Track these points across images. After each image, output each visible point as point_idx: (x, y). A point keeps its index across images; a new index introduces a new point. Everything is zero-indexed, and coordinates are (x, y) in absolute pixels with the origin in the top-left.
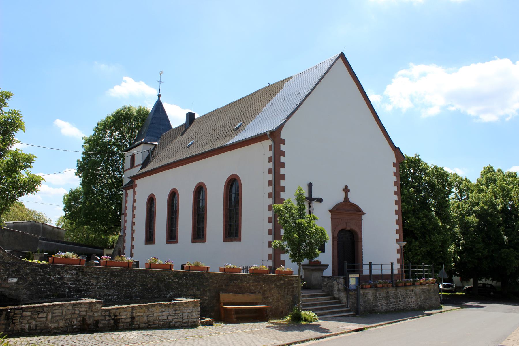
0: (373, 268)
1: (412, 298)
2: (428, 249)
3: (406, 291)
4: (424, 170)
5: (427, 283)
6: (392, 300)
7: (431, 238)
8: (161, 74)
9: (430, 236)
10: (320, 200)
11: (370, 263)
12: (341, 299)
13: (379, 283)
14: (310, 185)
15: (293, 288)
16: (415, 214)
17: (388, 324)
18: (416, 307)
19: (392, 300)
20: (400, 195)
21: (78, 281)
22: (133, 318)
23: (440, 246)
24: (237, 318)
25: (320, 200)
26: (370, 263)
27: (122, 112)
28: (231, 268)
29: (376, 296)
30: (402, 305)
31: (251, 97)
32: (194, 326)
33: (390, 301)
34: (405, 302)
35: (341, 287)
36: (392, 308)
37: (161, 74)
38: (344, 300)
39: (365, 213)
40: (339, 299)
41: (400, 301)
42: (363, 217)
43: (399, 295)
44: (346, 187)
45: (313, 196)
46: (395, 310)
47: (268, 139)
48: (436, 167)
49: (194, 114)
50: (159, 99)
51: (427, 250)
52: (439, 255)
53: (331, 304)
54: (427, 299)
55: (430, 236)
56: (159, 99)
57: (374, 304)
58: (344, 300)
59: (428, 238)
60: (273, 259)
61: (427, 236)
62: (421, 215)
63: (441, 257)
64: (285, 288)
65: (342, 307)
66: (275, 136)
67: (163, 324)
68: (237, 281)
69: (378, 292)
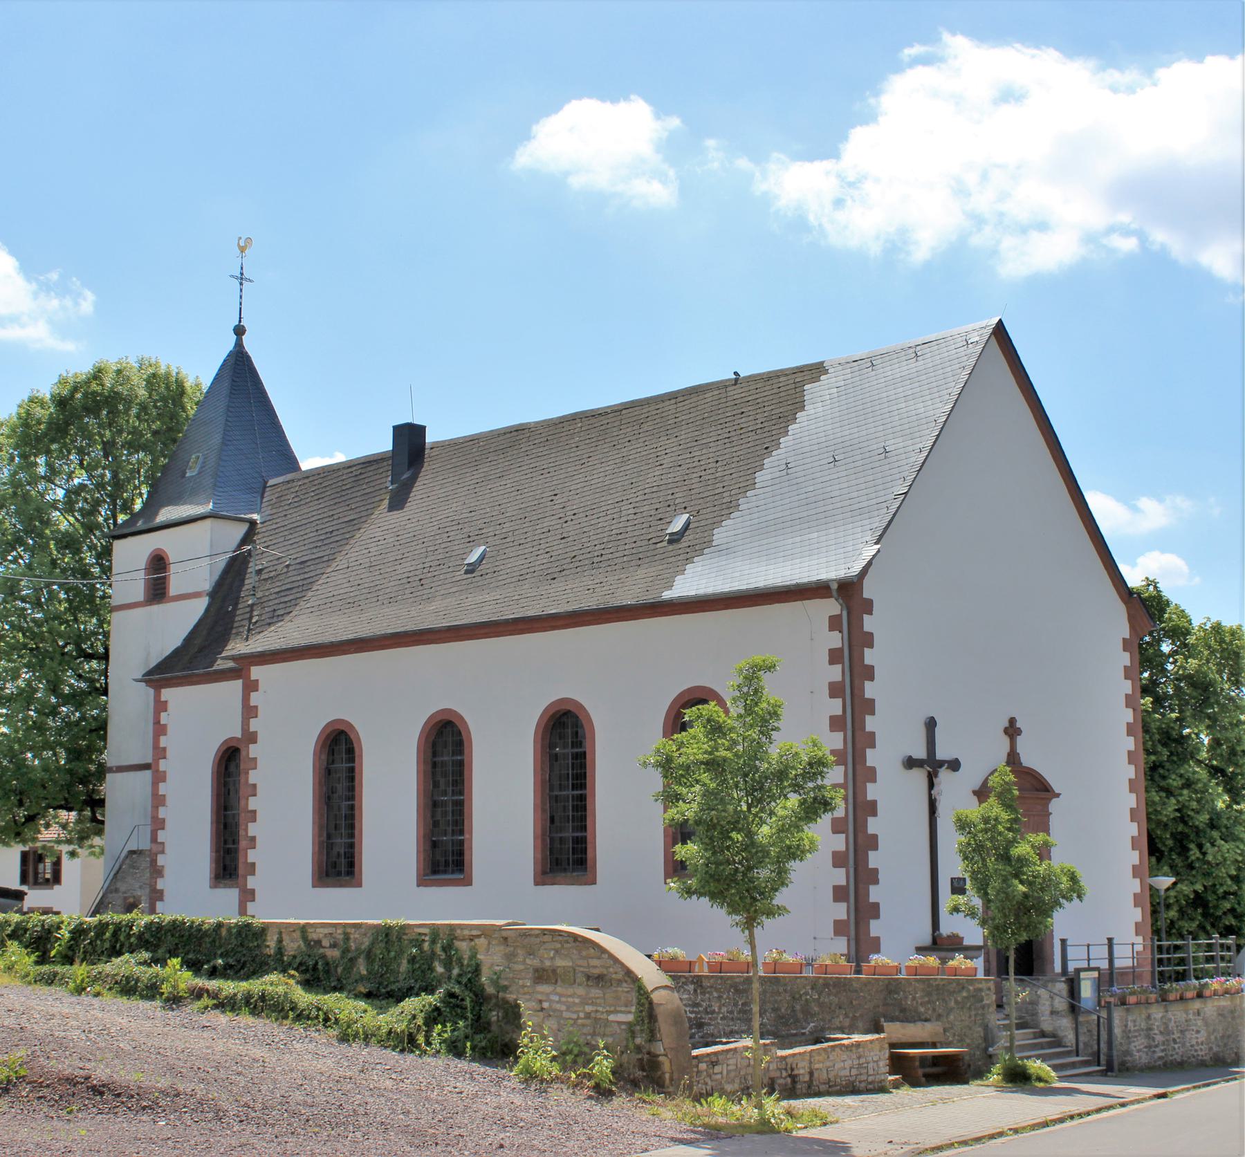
0: (1116, 954)
1: (1198, 1032)
2: (1199, 887)
3: (1187, 1012)
4: (1179, 633)
5: (1227, 992)
6: (1159, 1038)
7: (1204, 854)
8: (242, 250)
9: (1200, 846)
10: (954, 765)
11: (1110, 940)
12: (1061, 1034)
13: (1131, 994)
14: (931, 724)
15: (983, 1007)
16: (1157, 778)
17: (1194, 1087)
18: (1207, 1058)
19: (1159, 1038)
20: (1140, 734)
21: (697, 1005)
22: (811, 1074)
23: (1232, 877)
24: (926, 1076)
25: (954, 765)
26: (1110, 940)
27: (94, 387)
28: (884, 966)
29: (1126, 1026)
30: (1177, 1053)
31: (669, 406)
32: (882, 1089)
33: (1154, 1039)
34: (1184, 1045)
35: (1061, 1004)
36: (1160, 1058)
37: (242, 250)
38: (1070, 1037)
39: (1058, 795)
40: (1054, 1036)
41: (1174, 1040)
42: (1054, 805)
43: (1172, 1024)
44: (1012, 721)
45: (940, 755)
46: (1165, 1064)
47: (831, 597)
48: (1217, 629)
49: (422, 430)
50: (239, 344)
51: (1195, 891)
52: (1228, 905)
53: (1043, 1048)
54: (1229, 1036)
55: (1200, 846)
56: (239, 344)
57: (1125, 1048)
58: (1070, 1037)
59: (1194, 853)
60: (853, 933)
61: (1192, 846)
62: (1174, 782)
63: (1232, 910)
64: (970, 1008)
65: (1068, 1054)
66: (849, 592)
67: (847, 1086)
68: (897, 993)
69: (1130, 1018)
